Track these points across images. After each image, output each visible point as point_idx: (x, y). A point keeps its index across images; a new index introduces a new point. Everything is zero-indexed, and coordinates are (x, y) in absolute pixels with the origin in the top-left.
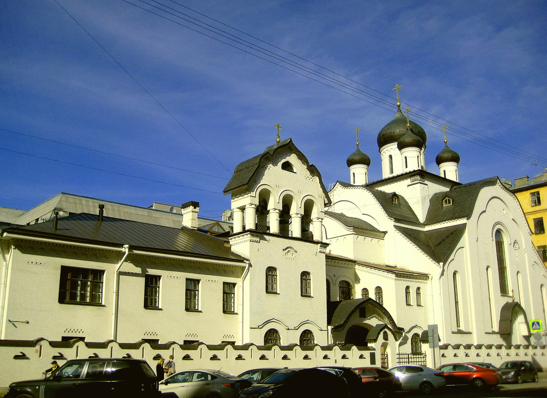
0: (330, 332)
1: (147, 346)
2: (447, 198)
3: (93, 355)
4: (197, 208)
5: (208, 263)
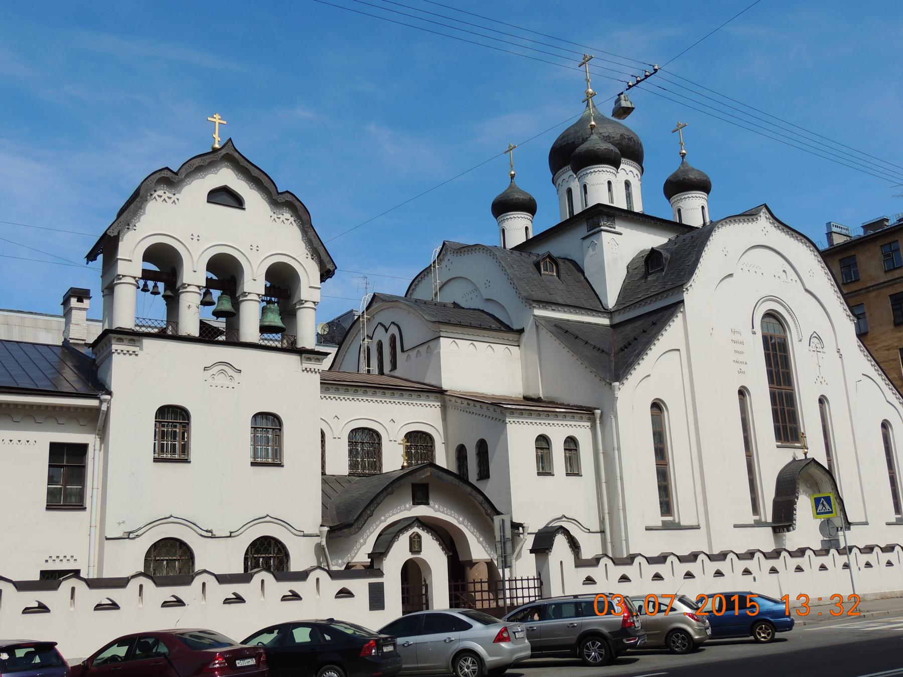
3: (289, 592)
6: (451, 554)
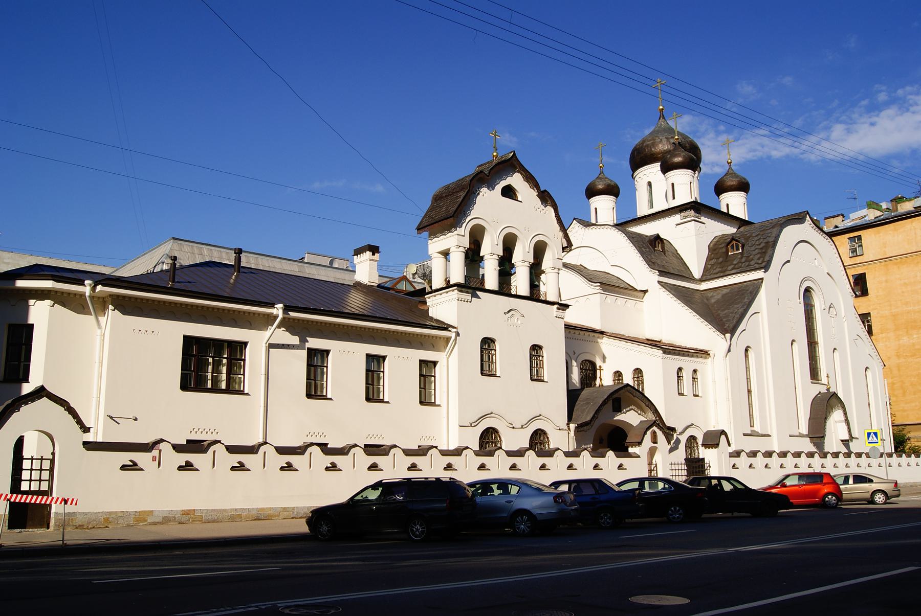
0: (572, 433)
1: (316, 450)
2: (734, 242)
4: (377, 255)
5: (398, 332)
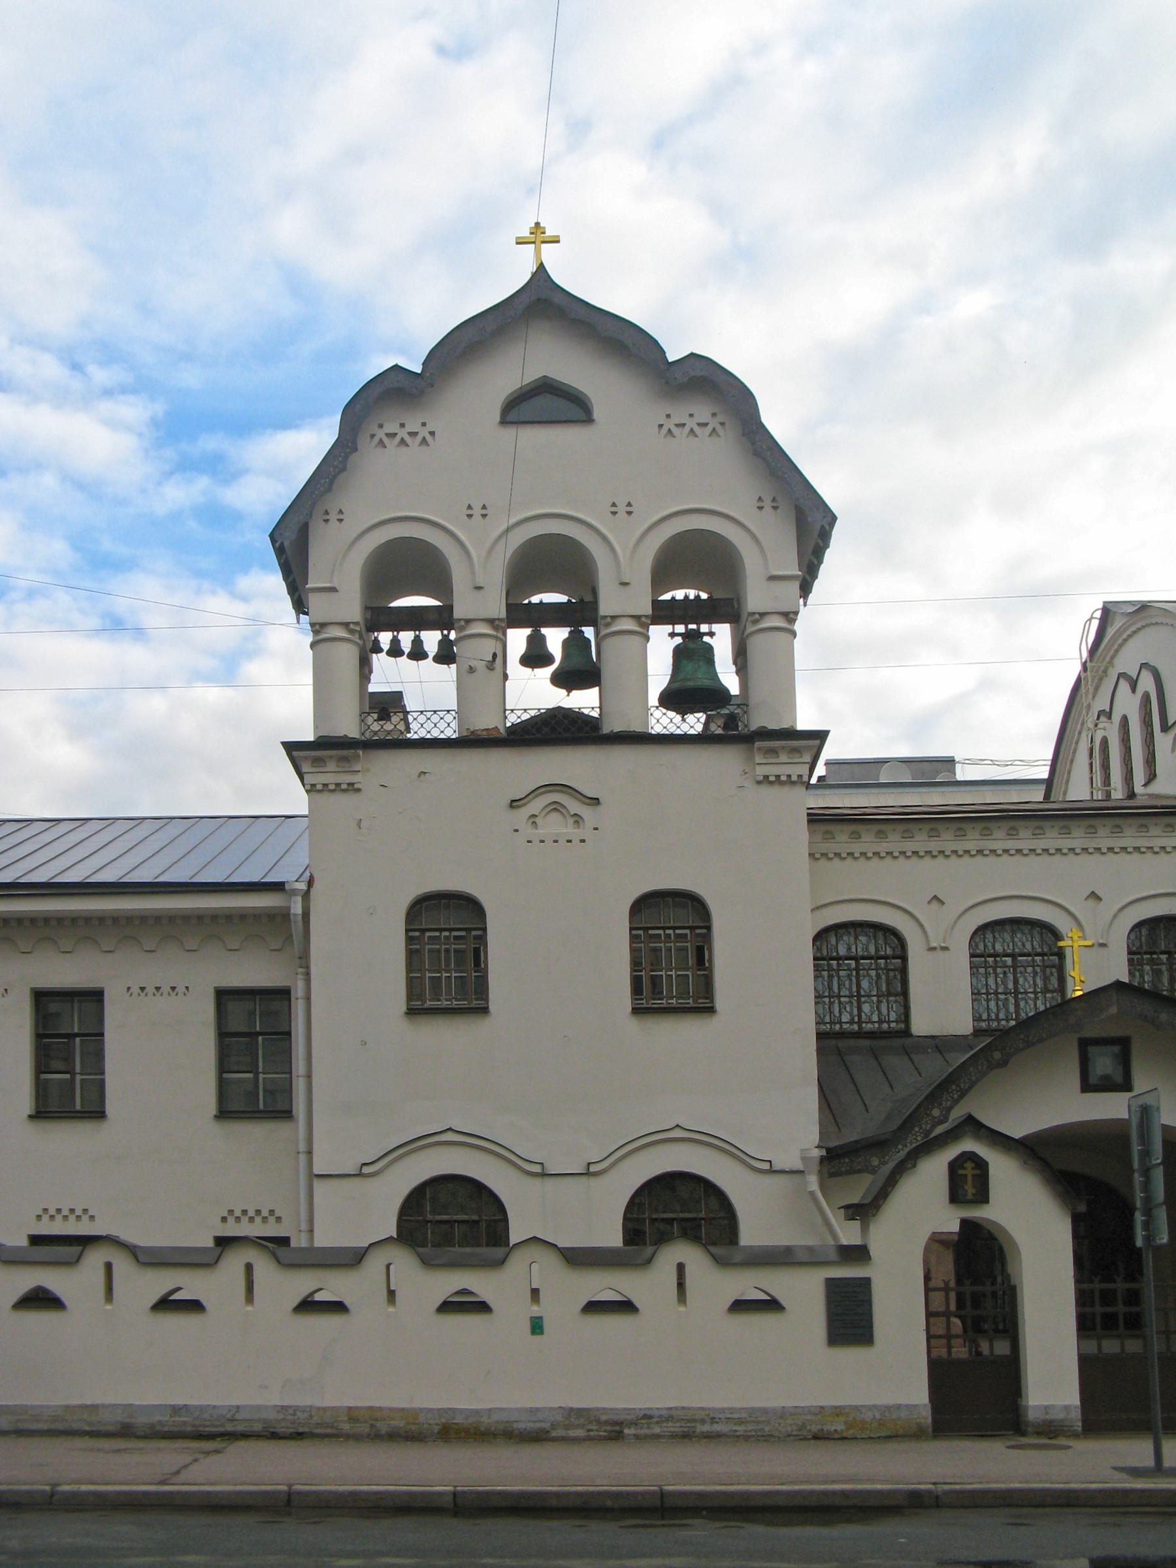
6: (1082, 1208)
